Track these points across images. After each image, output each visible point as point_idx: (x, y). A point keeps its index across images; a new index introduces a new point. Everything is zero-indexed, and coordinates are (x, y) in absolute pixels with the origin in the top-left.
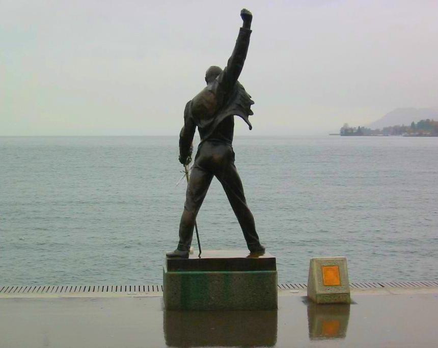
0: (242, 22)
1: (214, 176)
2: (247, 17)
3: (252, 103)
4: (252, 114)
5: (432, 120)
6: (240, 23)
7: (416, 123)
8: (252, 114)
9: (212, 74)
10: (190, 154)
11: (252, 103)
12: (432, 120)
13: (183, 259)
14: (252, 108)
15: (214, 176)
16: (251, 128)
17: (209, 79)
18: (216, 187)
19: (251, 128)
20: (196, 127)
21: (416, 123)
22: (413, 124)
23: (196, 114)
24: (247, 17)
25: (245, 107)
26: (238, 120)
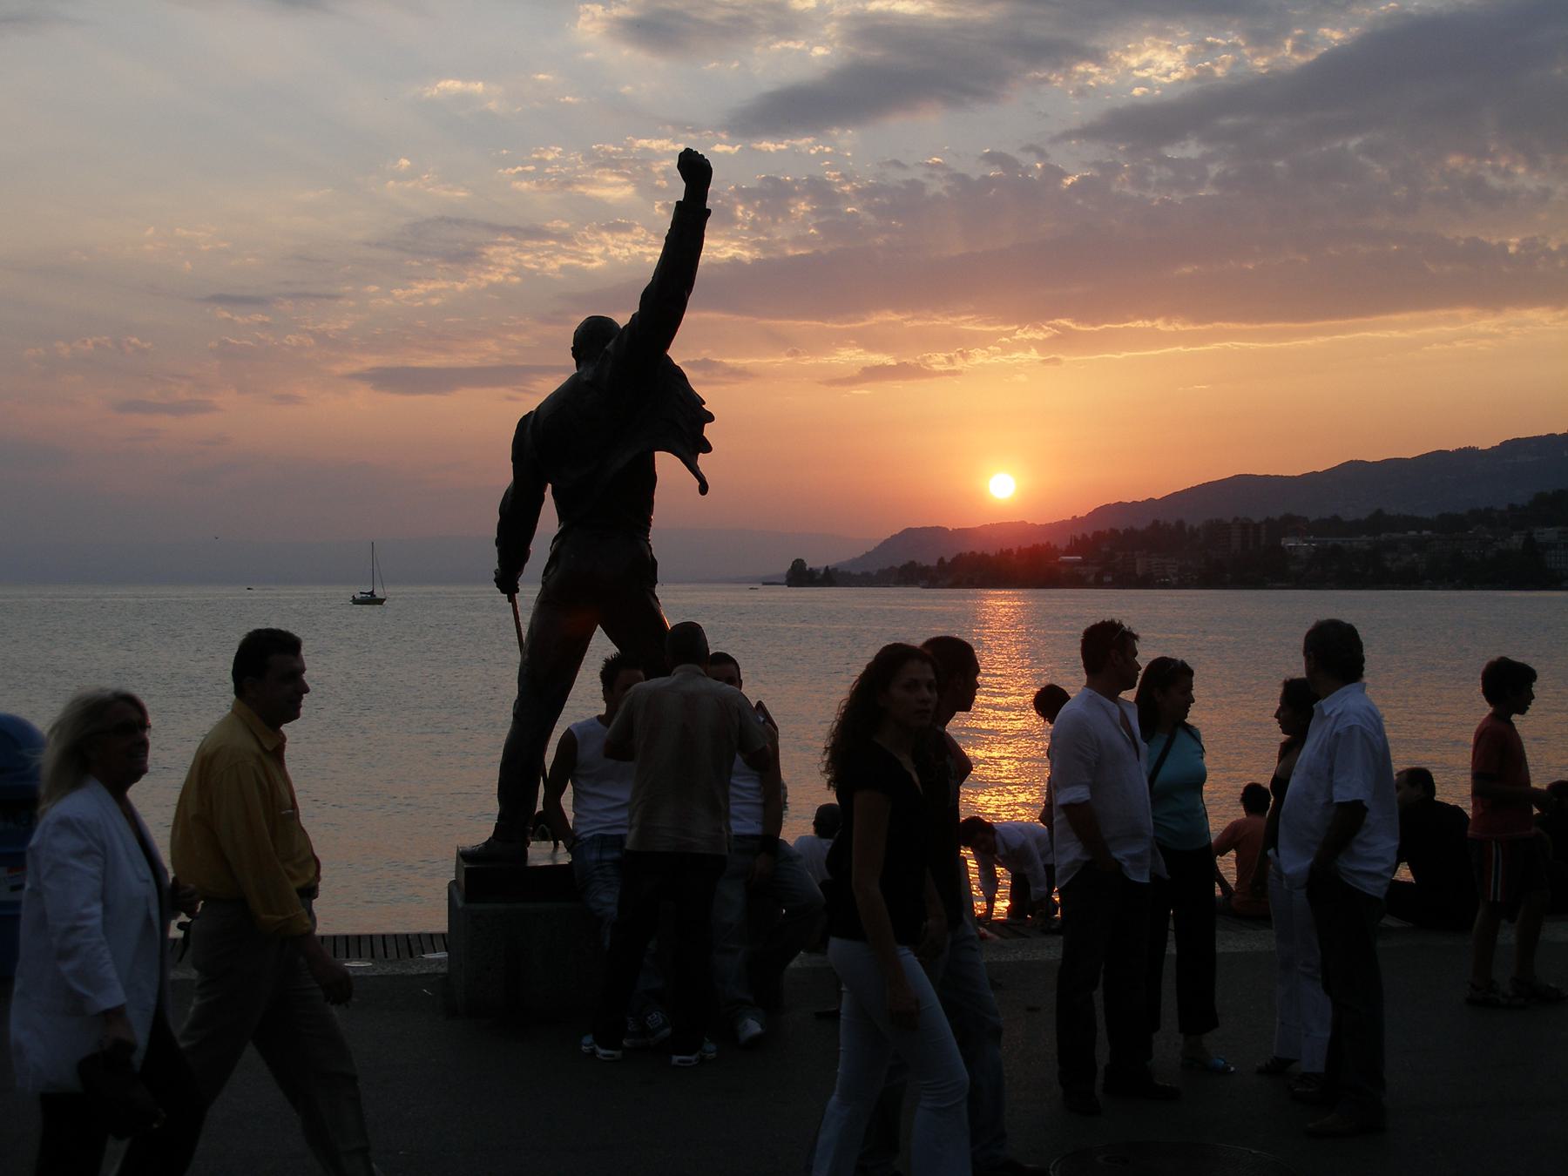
0: (681, 186)
3: (710, 417)
4: (707, 448)
5: (826, 771)
6: (677, 189)
7: (948, 560)
8: (707, 448)
9: (593, 337)
10: (524, 555)
11: (710, 417)
12: (826, 771)
13: (809, 361)
14: (709, 431)
16: (704, 489)
17: (313, 864)
19: (704, 489)
20: (544, 489)
21: (948, 560)
22: (941, 560)
23: (543, 444)
25: (685, 424)
26: (667, 464)
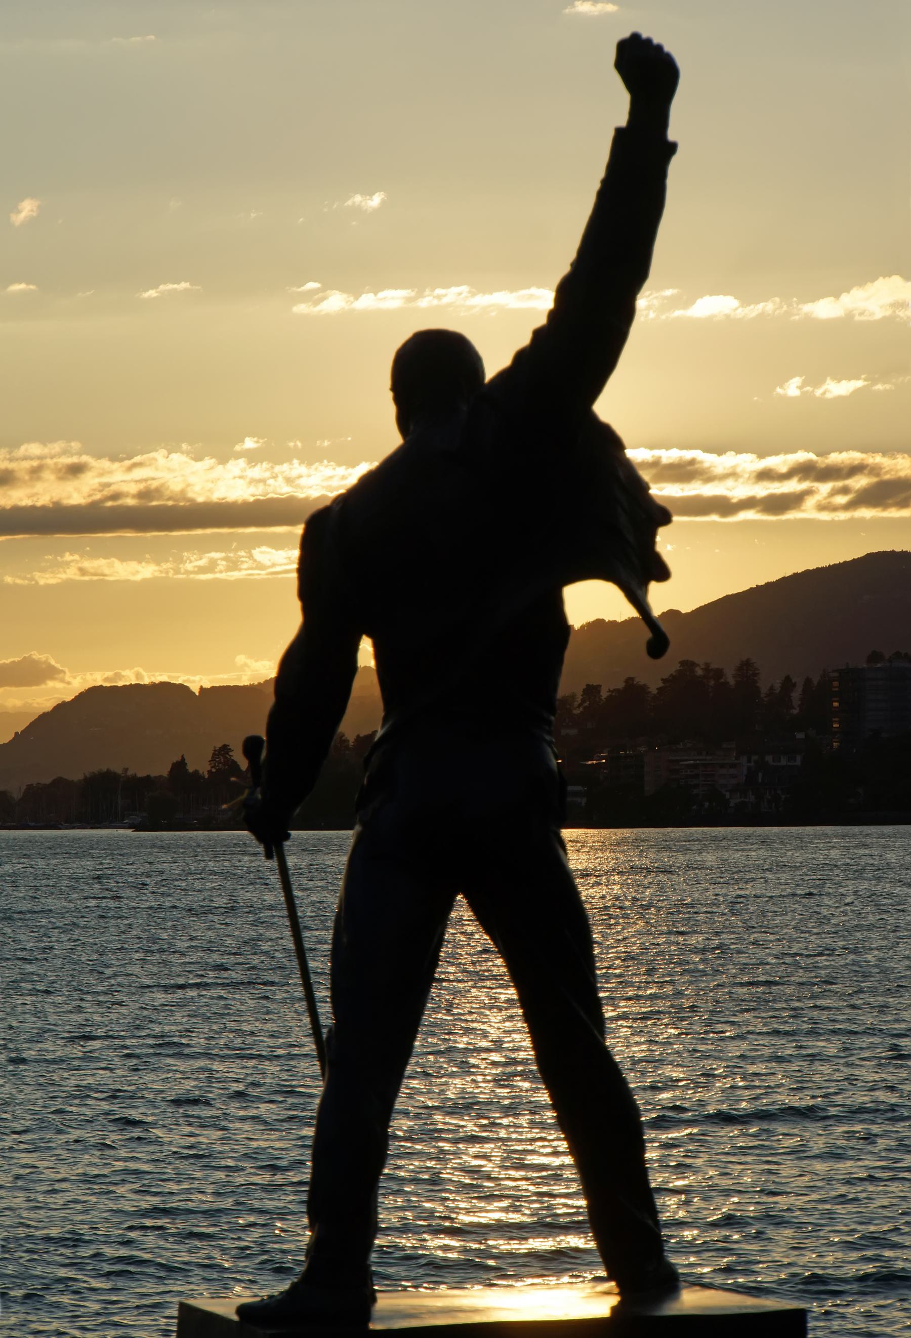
1: (462, 910)
2: (647, 70)
6: (615, 106)
15: (462, 910)
18: (477, 1014)
24: (647, 70)
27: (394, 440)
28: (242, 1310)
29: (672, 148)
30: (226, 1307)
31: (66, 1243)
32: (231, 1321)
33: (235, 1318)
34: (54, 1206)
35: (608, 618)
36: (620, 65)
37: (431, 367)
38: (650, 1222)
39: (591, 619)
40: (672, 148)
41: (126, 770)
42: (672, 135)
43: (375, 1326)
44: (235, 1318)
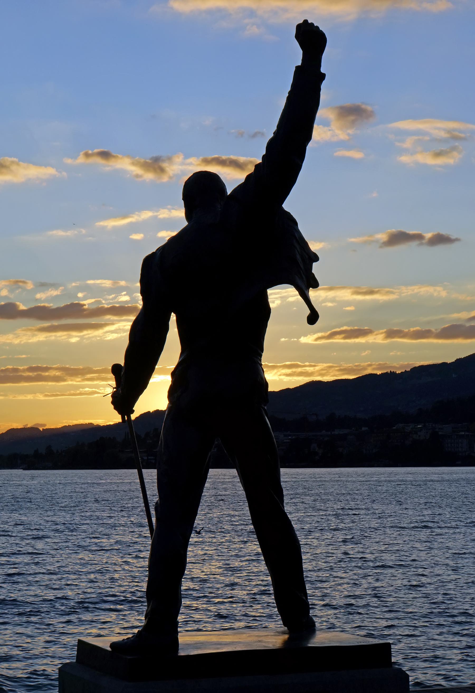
2: (311, 38)
6: (296, 56)
24: (311, 38)
27: (185, 223)
28: (113, 645)
29: (323, 76)
30: (104, 643)
31: (113, 599)
32: (107, 651)
33: (109, 649)
34: (54, 587)
35: (160, 409)
36: (298, 37)
37: (201, 191)
38: (304, 598)
39: (155, 409)
40: (323, 76)
41: (27, 425)
42: (323, 70)
43: (182, 653)
44: (109, 649)
